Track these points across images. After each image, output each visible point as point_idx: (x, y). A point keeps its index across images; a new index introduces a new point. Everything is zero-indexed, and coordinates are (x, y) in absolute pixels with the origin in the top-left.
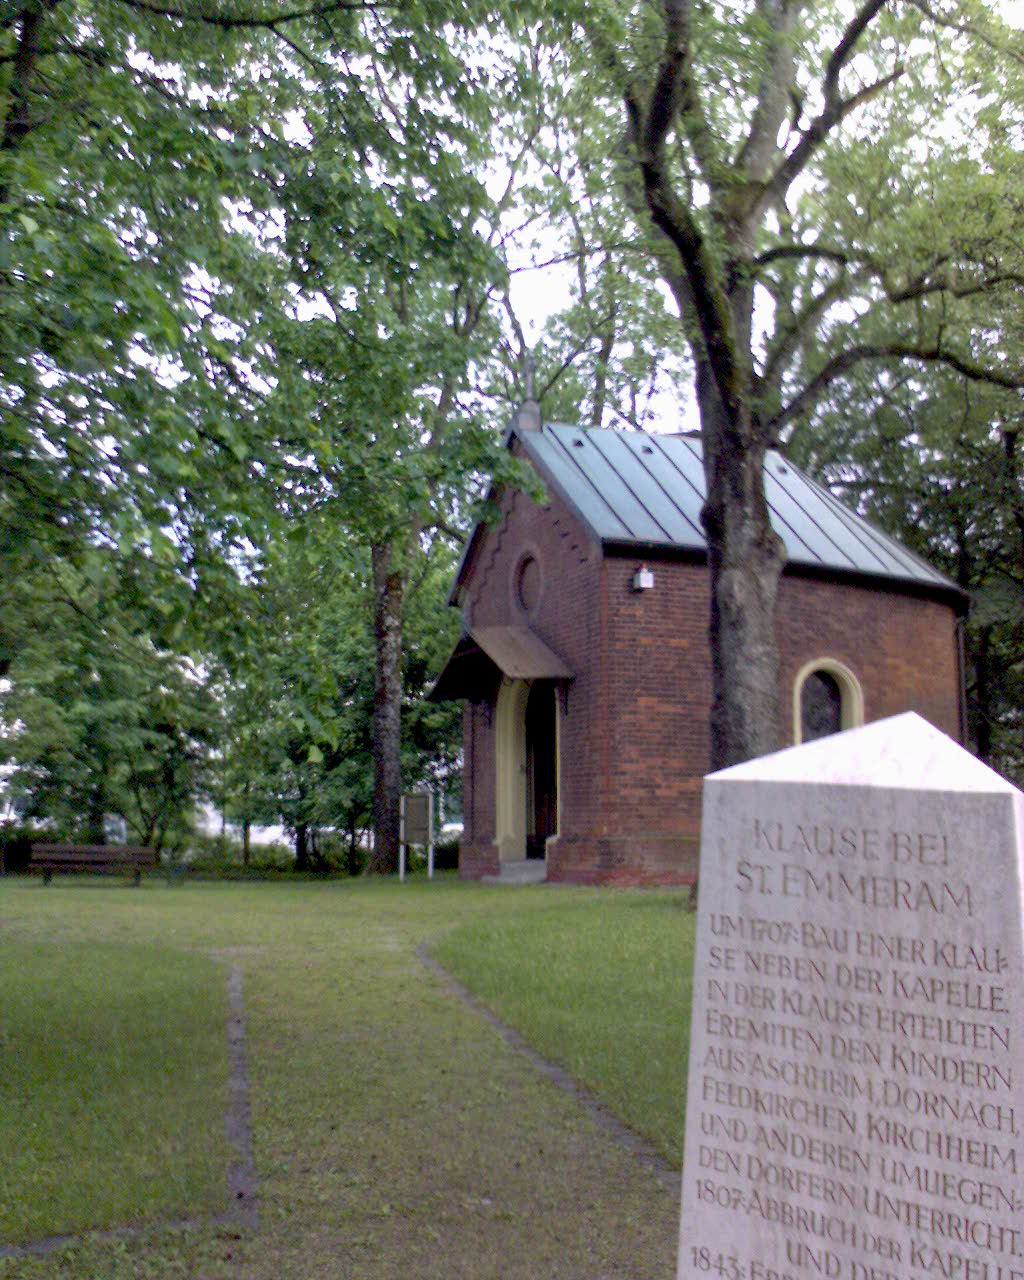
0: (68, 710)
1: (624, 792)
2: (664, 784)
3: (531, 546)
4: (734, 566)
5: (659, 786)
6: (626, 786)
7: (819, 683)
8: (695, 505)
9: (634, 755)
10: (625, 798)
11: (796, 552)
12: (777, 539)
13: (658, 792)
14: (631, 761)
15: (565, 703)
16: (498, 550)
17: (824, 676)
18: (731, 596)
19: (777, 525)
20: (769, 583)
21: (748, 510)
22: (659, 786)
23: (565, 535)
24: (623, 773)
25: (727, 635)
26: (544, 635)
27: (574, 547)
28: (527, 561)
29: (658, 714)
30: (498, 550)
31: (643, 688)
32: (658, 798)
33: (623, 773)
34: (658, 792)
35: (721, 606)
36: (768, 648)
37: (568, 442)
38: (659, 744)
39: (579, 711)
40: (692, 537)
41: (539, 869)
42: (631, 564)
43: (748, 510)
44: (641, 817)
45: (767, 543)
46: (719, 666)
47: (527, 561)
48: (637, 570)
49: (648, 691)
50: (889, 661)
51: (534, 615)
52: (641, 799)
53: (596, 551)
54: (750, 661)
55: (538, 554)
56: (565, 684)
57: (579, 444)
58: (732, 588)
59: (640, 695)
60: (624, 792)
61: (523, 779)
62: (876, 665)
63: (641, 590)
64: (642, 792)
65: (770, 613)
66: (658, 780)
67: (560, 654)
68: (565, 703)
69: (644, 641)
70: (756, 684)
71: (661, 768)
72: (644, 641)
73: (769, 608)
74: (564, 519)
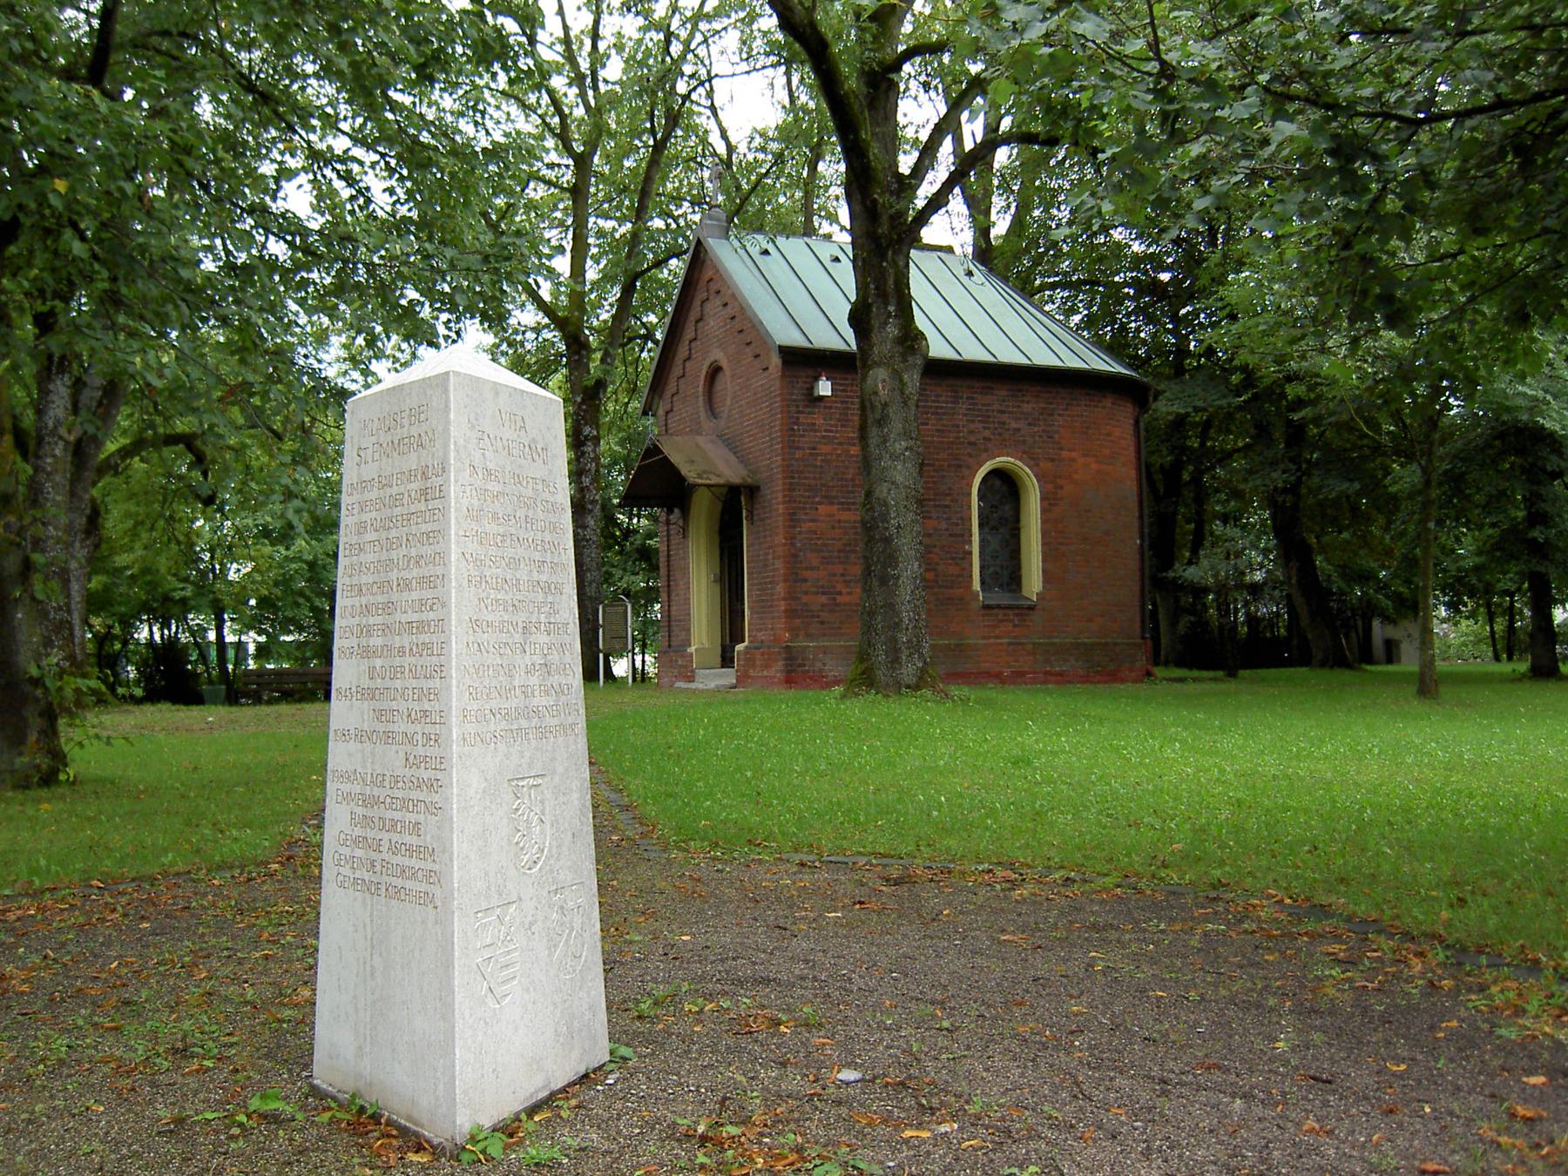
0: (287, 549)
1: (805, 599)
2: (844, 591)
3: (717, 355)
4: (878, 365)
5: (840, 593)
6: (806, 593)
7: (998, 483)
8: (841, 311)
9: (815, 563)
10: (806, 604)
11: (938, 349)
12: (921, 336)
13: (839, 599)
14: (812, 569)
15: (750, 512)
16: (689, 358)
17: (998, 474)
18: (876, 393)
19: (920, 322)
20: (913, 379)
21: (891, 308)
22: (840, 593)
23: (748, 344)
24: (805, 580)
25: (874, 432)
26: (731, 444)
27: (757, 356)
28: (715, 371)
29: (839, 521)
30: (689, 358)
31: (823, 497)
32: (837, 605)
33: (805, 580)
34: (839, 599)
35: (867, 404)
36: (911, 443)
37: (754, 252)
38: (839, 551)
39: (763, 520)
40: (841, 338)
41: (728, 677)
42: (811, 372)
43: (891, 308)
44: (822, 623)
45: (911, 339)
46: (866, 463)
47: (715, 371)
48: (817, 379)
49: (830, 500)
50: (1064, 453)
51: (722, 423)
52: (823, 605)
53: (775, 360)
54: (894, 457)
55: (724, 363)
56: (753, 491)
57: (766, 252)
58: (877, 386)
59: (820, 503)
60: (805, 599)
61: (717, 588)
62: (1053, 460)
63: (822, 398)
64: (823, 599)
65: (913, 408)
66: (839, 587)
67: (743, 460)
68: (750, 512)
69: (824, 449)
70: (899, 479)
71: (843, 575)
72: (824, 449)
73: (912, 403)
74: (746, 327)
